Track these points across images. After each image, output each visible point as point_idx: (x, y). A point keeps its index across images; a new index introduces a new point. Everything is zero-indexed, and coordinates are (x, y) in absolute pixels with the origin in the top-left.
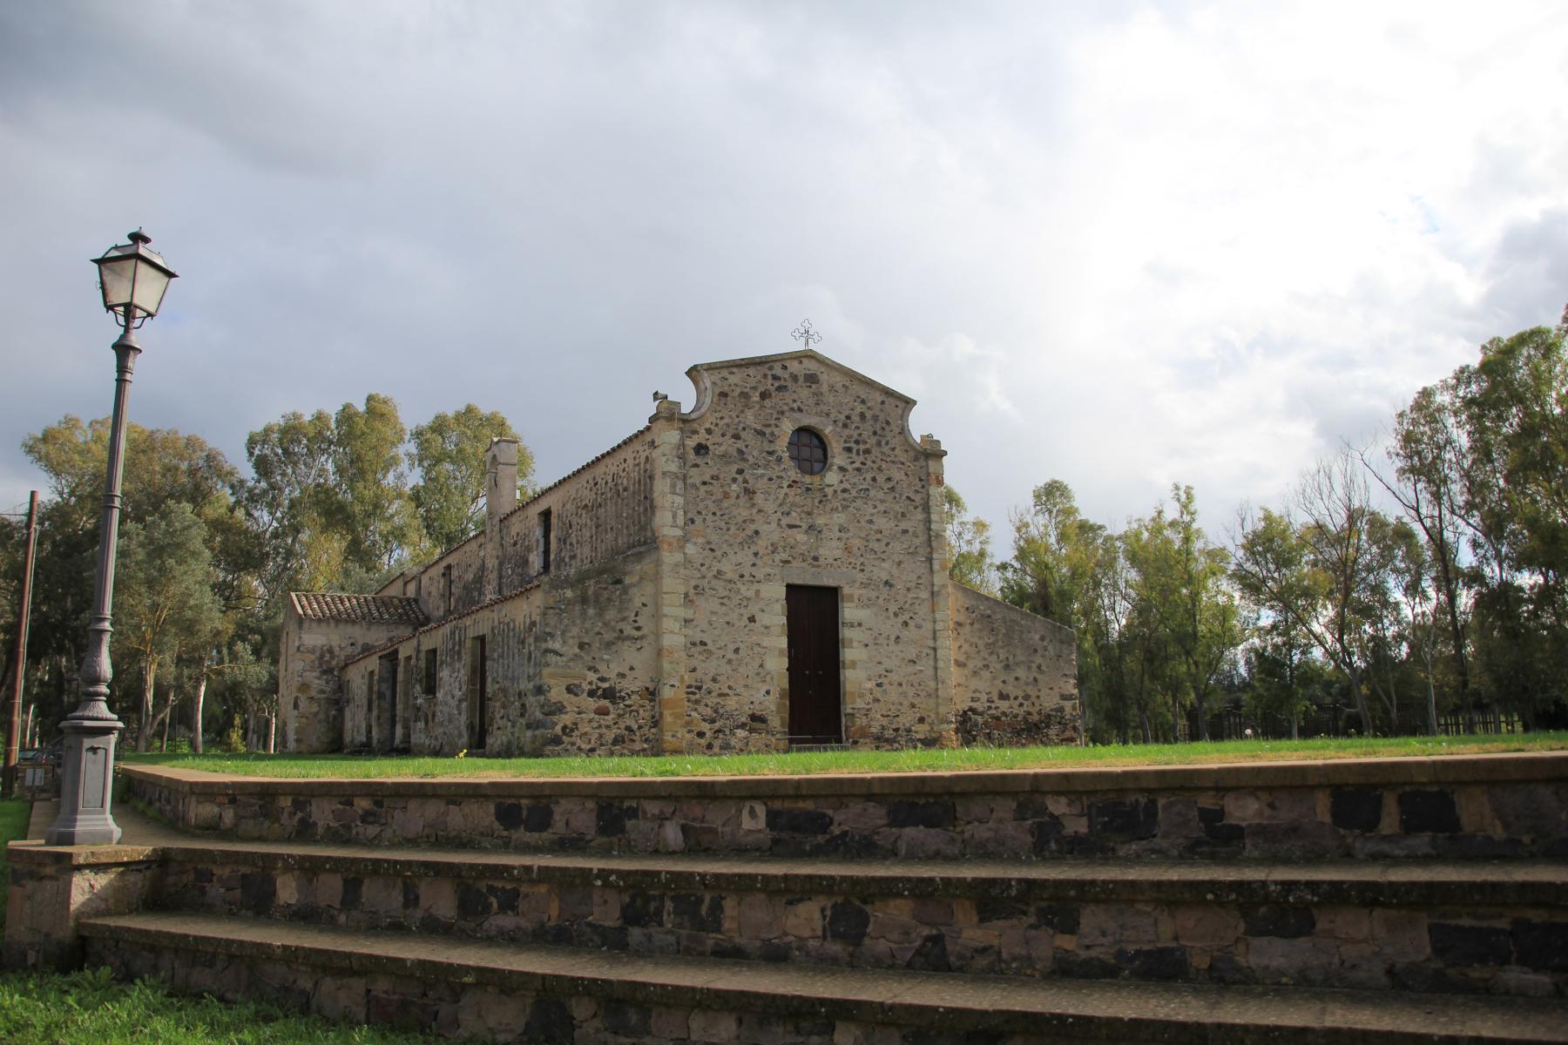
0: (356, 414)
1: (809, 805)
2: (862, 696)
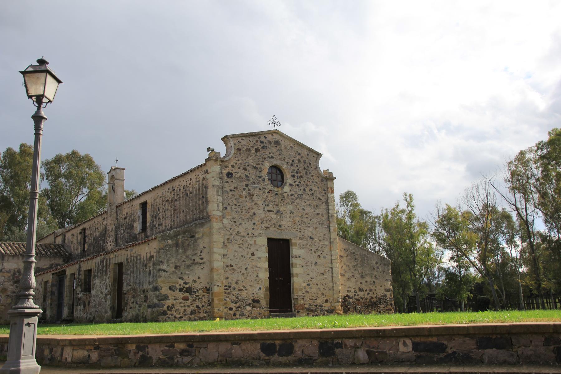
0: (15, 153)
1: (435, 339)
2: (301, 290)
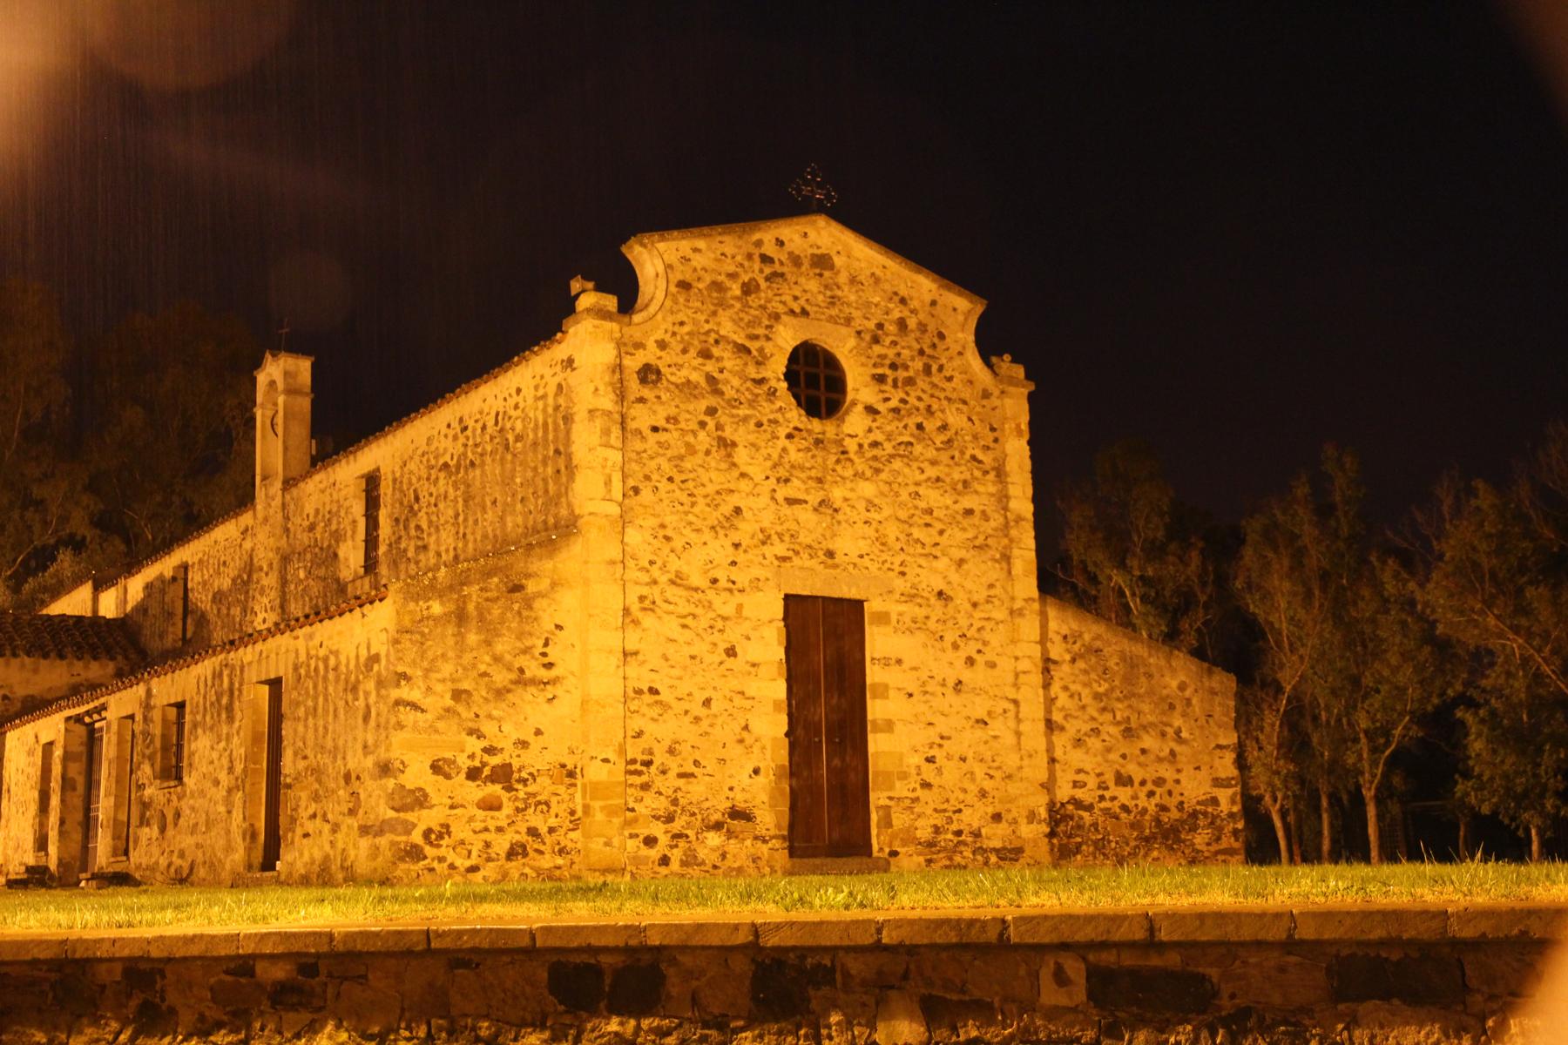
2: (904, 776)
